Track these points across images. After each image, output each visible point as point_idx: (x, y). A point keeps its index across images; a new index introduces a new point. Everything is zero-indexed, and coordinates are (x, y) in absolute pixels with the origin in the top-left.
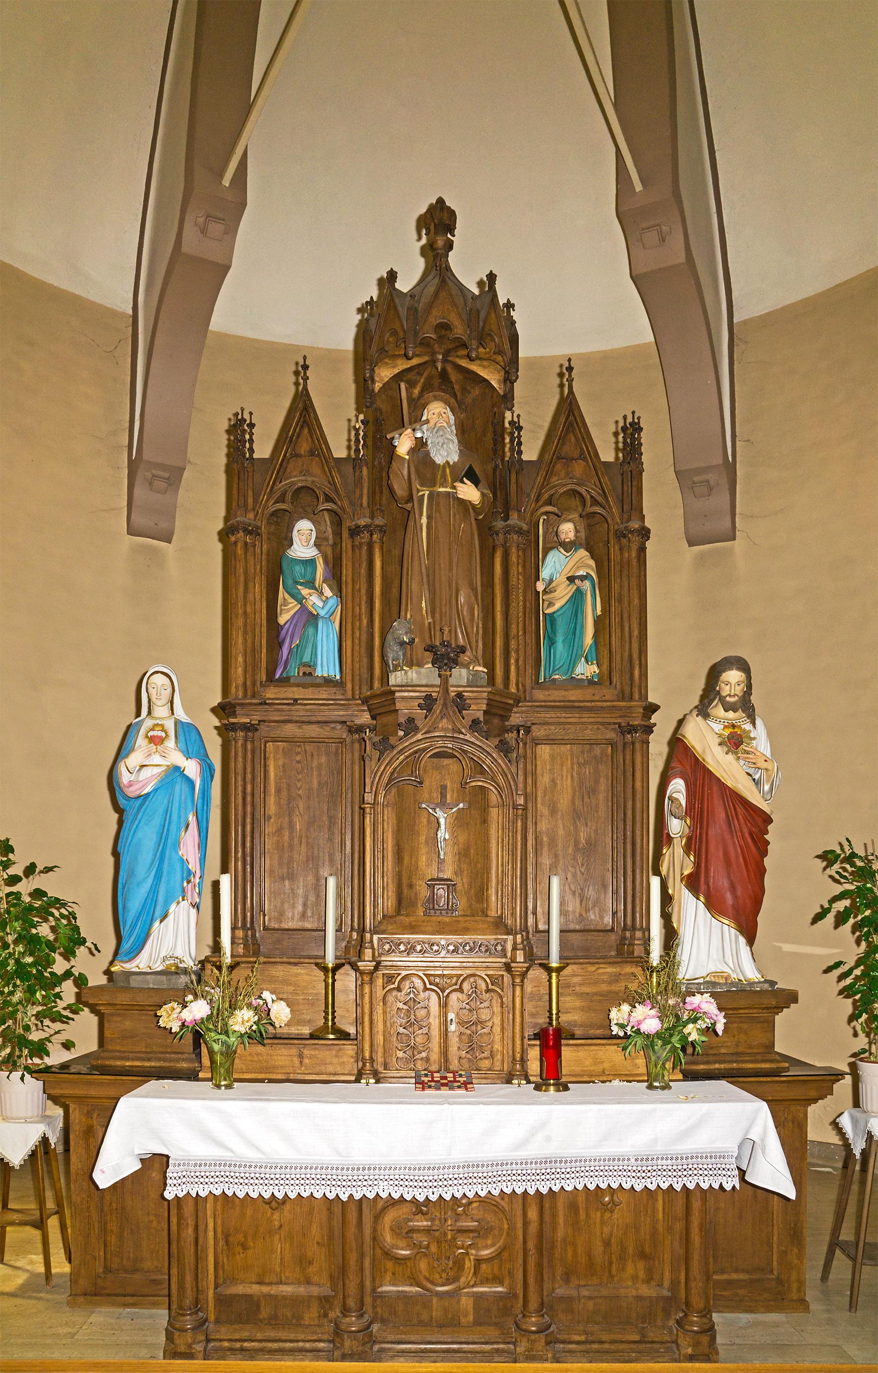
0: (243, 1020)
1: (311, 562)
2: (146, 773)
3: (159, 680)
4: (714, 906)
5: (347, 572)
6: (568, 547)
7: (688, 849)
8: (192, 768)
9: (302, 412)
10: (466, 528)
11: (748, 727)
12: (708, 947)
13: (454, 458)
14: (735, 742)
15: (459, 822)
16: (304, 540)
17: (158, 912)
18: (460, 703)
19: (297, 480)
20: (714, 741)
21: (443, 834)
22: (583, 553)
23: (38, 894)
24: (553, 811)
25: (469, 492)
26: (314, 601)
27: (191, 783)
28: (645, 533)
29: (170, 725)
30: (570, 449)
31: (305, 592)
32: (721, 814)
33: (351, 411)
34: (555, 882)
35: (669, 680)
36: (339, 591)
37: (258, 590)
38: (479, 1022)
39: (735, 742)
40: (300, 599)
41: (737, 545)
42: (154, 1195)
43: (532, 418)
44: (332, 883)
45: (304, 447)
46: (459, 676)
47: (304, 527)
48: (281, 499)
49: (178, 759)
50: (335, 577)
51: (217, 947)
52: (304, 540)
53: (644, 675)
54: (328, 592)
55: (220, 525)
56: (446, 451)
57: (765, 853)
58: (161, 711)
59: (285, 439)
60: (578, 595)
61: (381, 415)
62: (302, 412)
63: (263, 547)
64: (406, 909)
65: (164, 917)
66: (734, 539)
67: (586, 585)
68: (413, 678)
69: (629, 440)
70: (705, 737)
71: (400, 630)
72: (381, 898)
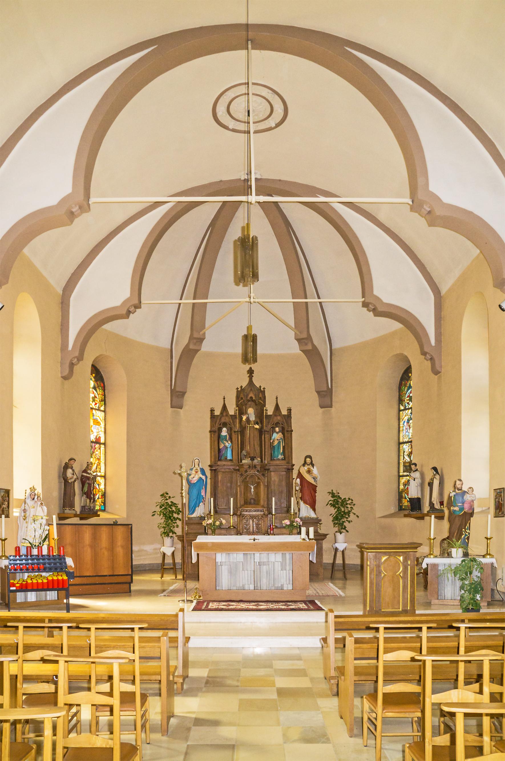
0: (218, 523)
1: (226, 436)
2: (194, 479)
3: (197, 460)
4: (305, 502)
5: (233, 439)
6: (277, 433)
7: (300, 492)
8: (203, 477)
9: (224, 408)
10: (257, 434)
11: (312, 468)
12: (306, 511)
13: (254, 419)
14: (309, 472)
15: (255, 488)
16: (224, 432)
17: (197, 505)
18: (255, 467)
19: (223, 420)
20: (305, 471)
21: (252, 490)
22: (280, 433)
23: (171, 502)
24: (274, 485)
25: (257, 426)
26: (227, 444)
27: (203, 480)
28: (292, 431)
29: (199, 469)
30: (277, 414)
31: (225, 442)
32: (306, 486)
33: (235, 406)
34: (274, 498)
35: (297, 459)
36: (232, 442)
37: (216, 443)
38: (260, 524)
39: (309, 472)
40: (224, 443)
41: (333, 410)
42: (190, 565)
43: (270, 409)
44: (232, 499)
45: (224, 414)
46: (255, 461)
47: (224, 429)
48: (220, 425)
49: (201, 476)
50: (231, 439)
51: (210, 512)
52: (224, 432)
53: (292, 458)
54: (229, 442)
55: (209, 429)
56: (253, 418)
57: (315, 492)
58: (197, 466)
59: (222, 413)
60: (279, 443)
61: (241, 411)
62: (224, 408)
63: (217, 434)
64: (247, 503)
65: (198, 506)
66: (332, 407)
67: (281, 441)
68: (246, 461)
69: (277, 436)
70: (304, 470)
71: (244, 452)
72: (241, 501)
